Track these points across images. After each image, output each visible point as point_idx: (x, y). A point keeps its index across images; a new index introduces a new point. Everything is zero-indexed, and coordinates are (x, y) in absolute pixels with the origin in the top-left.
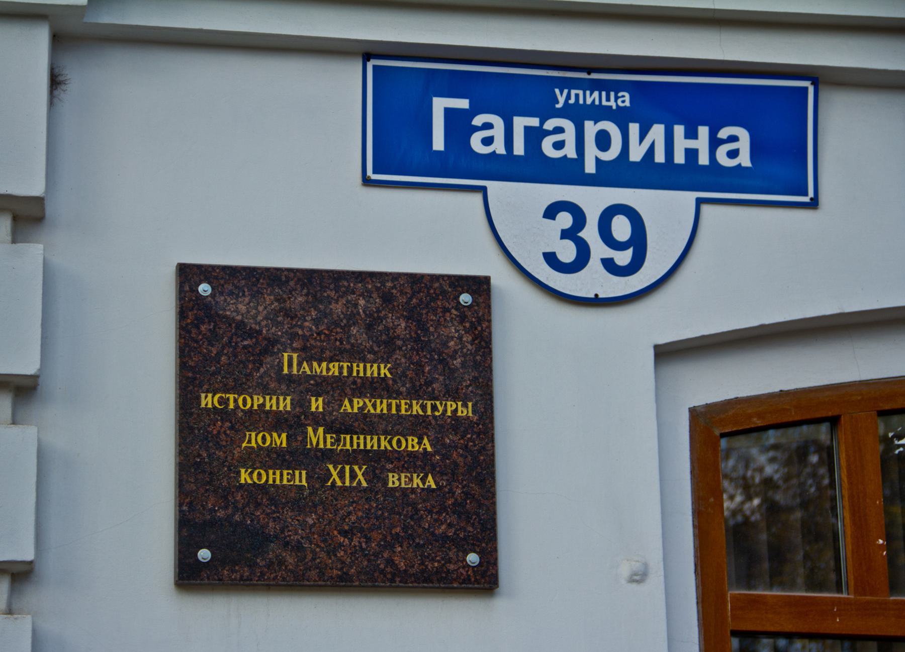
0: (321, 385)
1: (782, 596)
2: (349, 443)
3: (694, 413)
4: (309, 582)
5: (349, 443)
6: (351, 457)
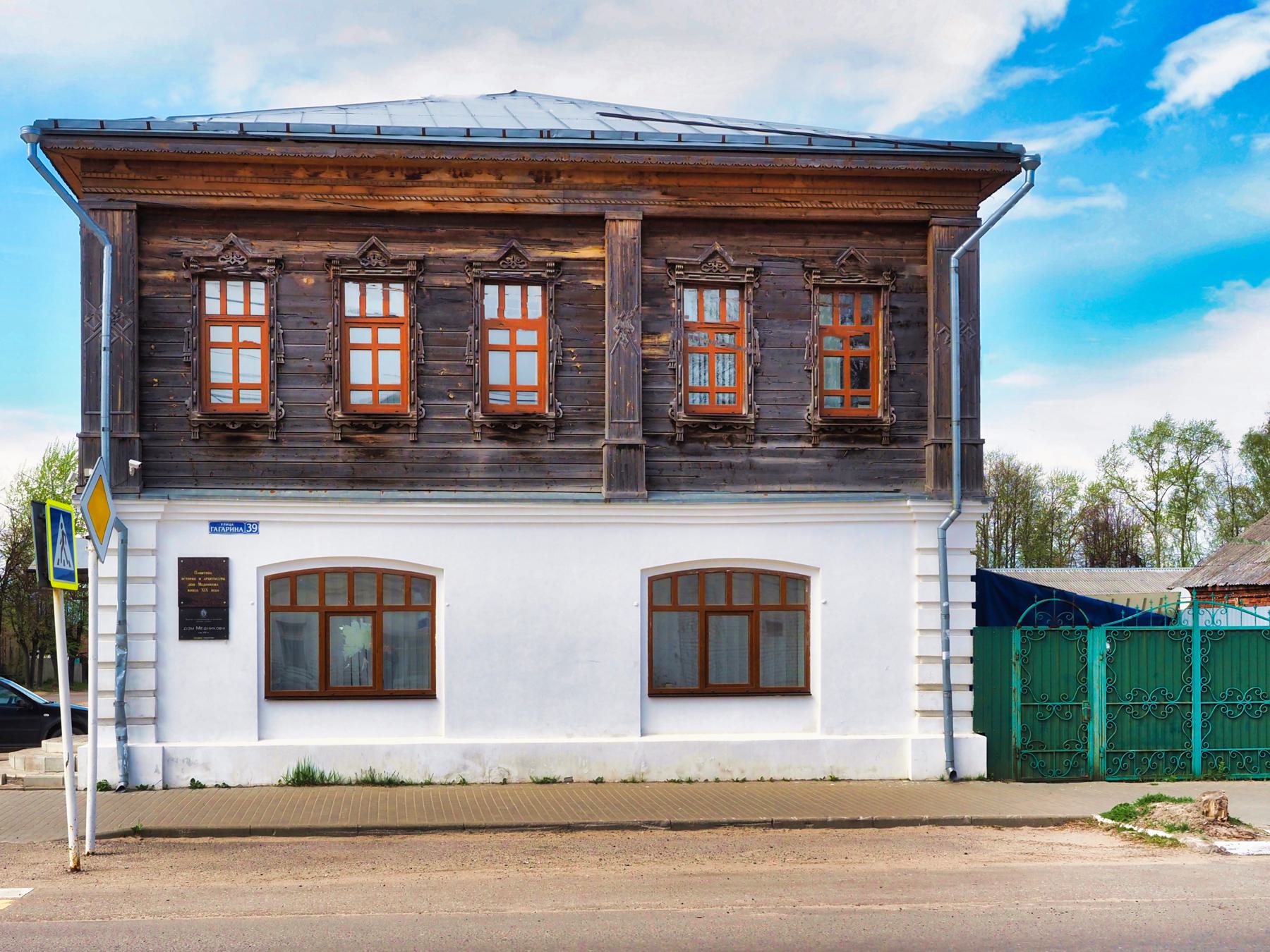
0: (200, 576)
1: (951, 470)
2: (205, 585)
3: (265, 577)
4: (1167, 573)
5: (205, 585)
6: (206, 587)
